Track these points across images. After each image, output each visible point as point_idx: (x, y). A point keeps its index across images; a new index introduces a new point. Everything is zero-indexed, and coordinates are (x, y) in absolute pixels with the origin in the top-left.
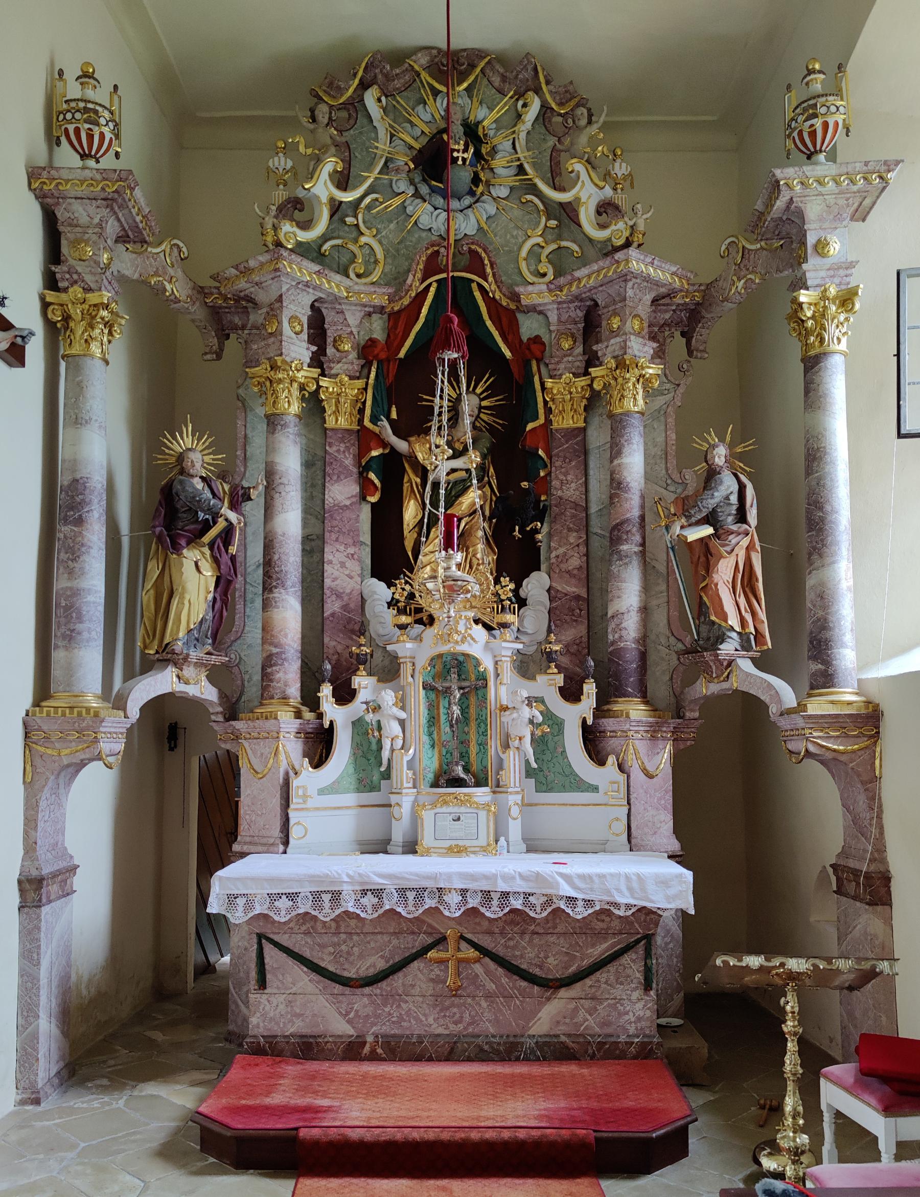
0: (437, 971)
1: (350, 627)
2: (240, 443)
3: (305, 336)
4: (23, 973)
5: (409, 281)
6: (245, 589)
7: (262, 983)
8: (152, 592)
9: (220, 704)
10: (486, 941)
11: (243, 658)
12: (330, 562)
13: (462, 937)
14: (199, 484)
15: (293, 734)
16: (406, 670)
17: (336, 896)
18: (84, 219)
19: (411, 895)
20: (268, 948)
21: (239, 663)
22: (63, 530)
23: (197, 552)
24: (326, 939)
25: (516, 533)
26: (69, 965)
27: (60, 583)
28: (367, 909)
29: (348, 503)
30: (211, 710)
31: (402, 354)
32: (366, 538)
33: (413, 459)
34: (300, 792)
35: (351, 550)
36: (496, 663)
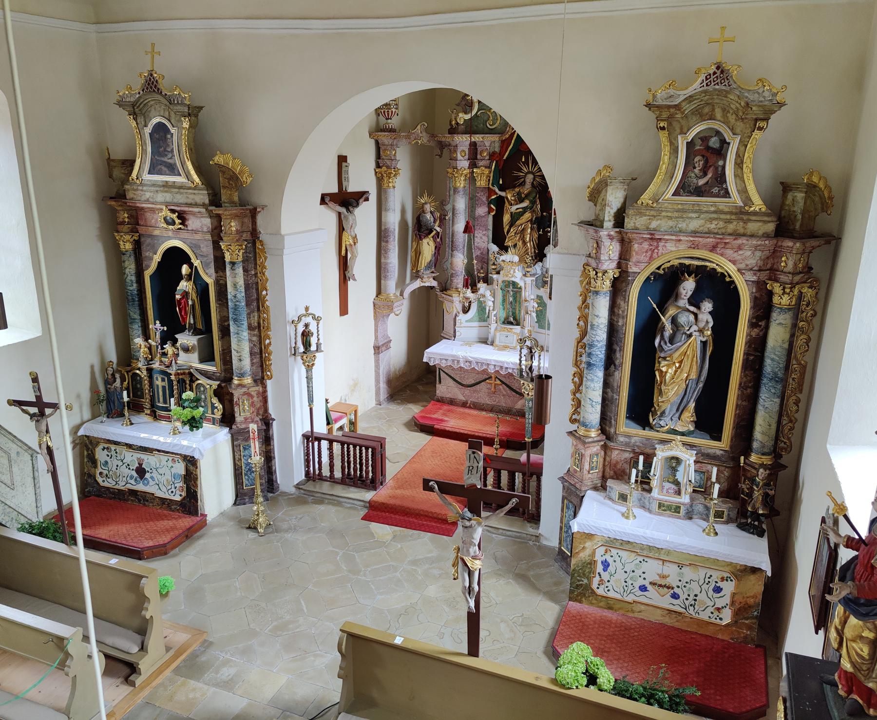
0: (489, 386)
1: (483, 260)
2: (448, 189)
3: (467, 157)
4: (375, 371)
5: (508, 130)
7: (440, 382)
10: (503, 380)
12: (477, 237)
13: (497, 377)
14: (428, 216)
16: (495, 283)
17: (458, 362)
18: (387, 143)
19: (480, 364)
20: (441, 372)
22: (383, 244)
23: (428, 239)
24: (457, 372)
25: (541, 233)
26: (390, 368)
27: (383, 260)
28: (466, 366)
29: (484, 215)
31: (505, 158)
32: (490, 227)
33: (507, 198)
34: (459, 321)
35: (484, 233)
36: (525, 284)
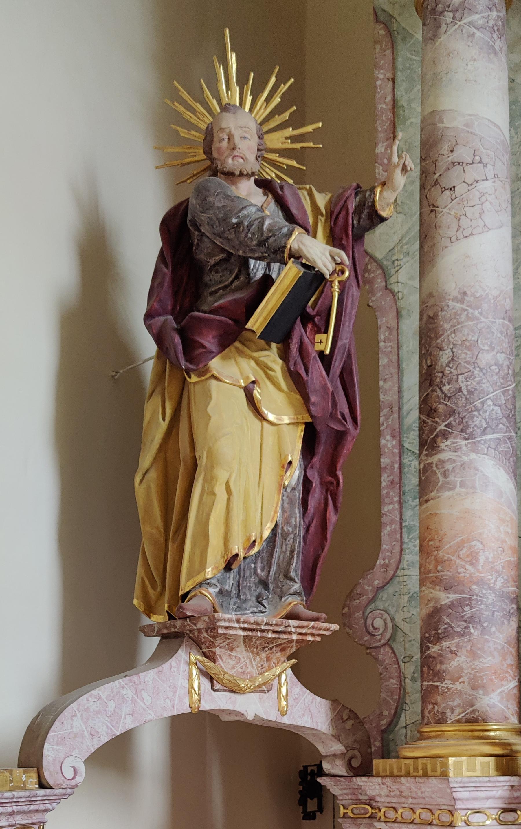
6: (401, 468)
8: (153, 475)
9: (337, 737)
11: (401, 625)
15: (494, 813)
21: (393, 637)
30: (322, 750)
